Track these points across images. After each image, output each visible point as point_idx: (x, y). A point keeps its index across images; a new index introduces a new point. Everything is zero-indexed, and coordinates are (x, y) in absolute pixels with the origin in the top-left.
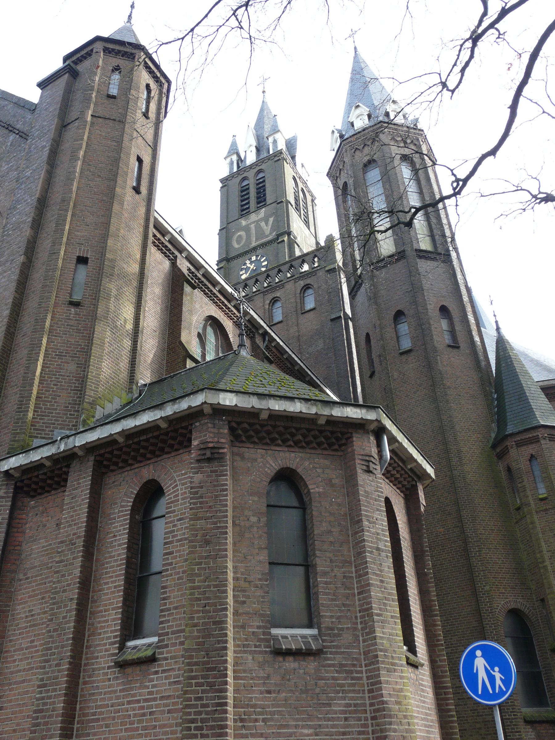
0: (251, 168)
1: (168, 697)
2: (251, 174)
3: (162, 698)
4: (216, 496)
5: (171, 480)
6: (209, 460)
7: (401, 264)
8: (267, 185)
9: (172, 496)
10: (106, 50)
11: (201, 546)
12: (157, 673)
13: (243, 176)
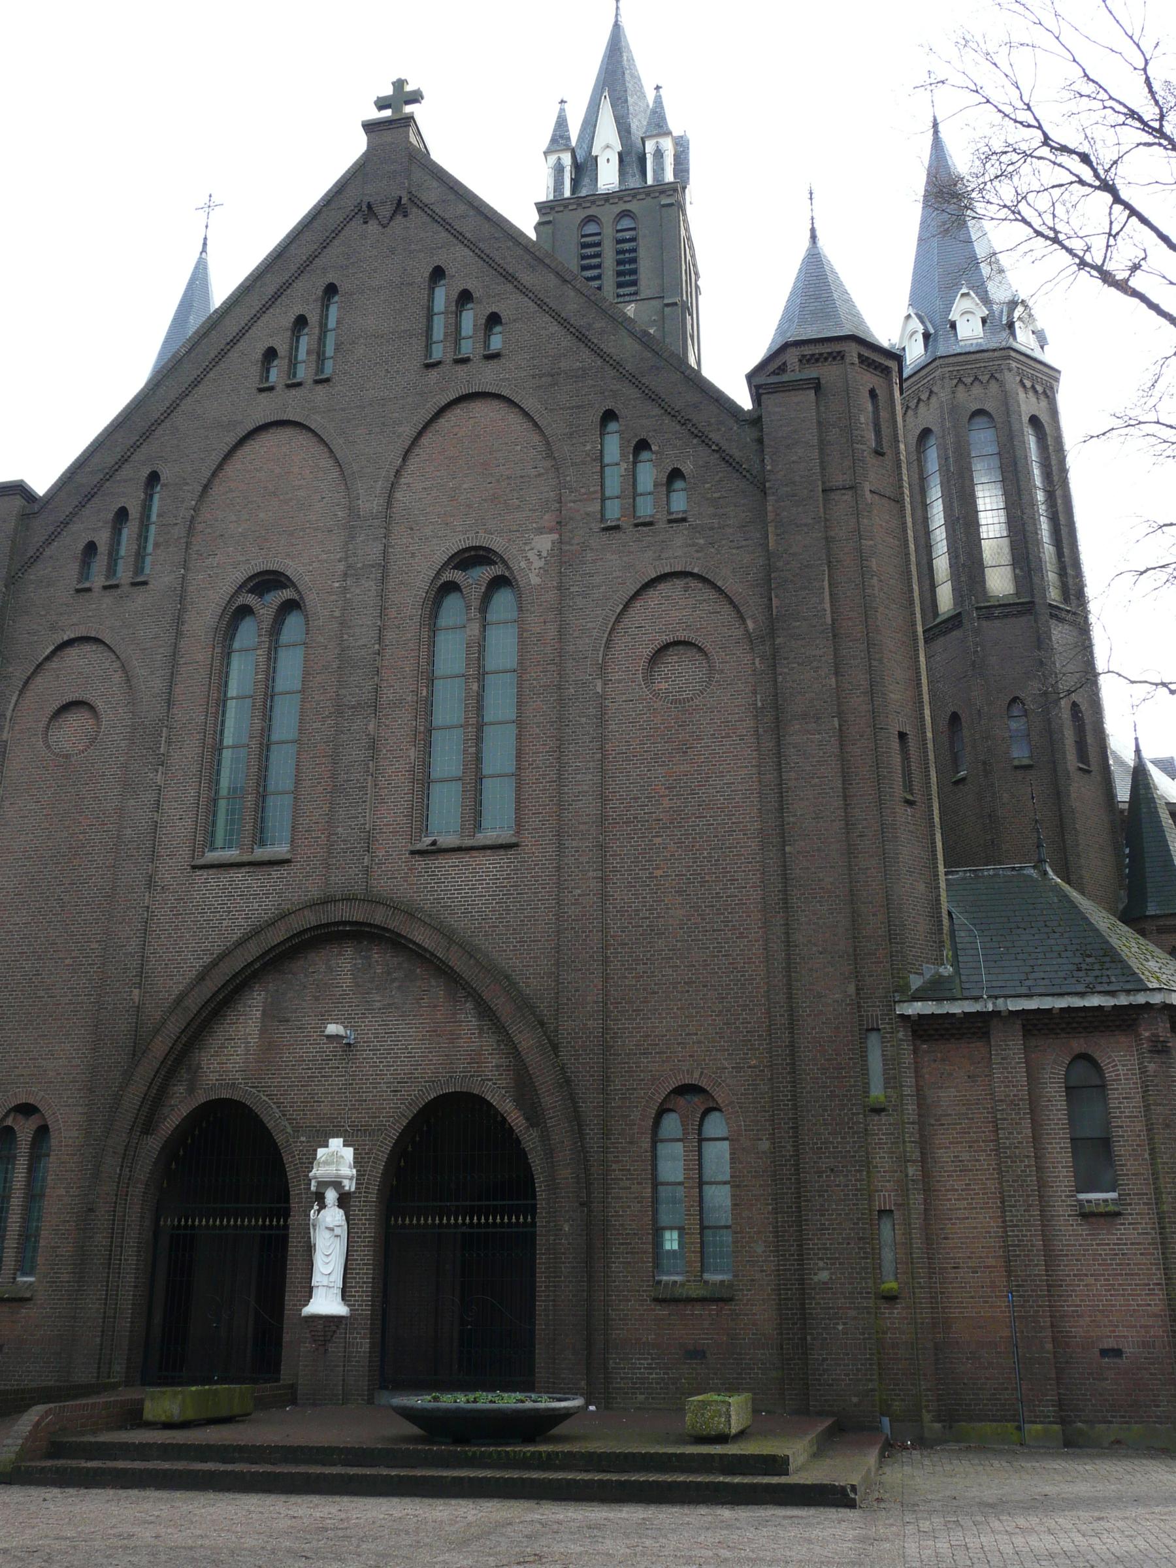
0: (607, 200)
1: (1138, 1244)
2: (607, 214)
3: (1132, 1244)
4: (1169, 1086)
5: (1109, 1058)
6: (1158, 1052)
7: (1023, 620)
8: (642, 253)
9: (1113, 1074)
10: (863, 359)
11: (1163, 1129)
12: (1123, 1224)
13: (590, 212)
